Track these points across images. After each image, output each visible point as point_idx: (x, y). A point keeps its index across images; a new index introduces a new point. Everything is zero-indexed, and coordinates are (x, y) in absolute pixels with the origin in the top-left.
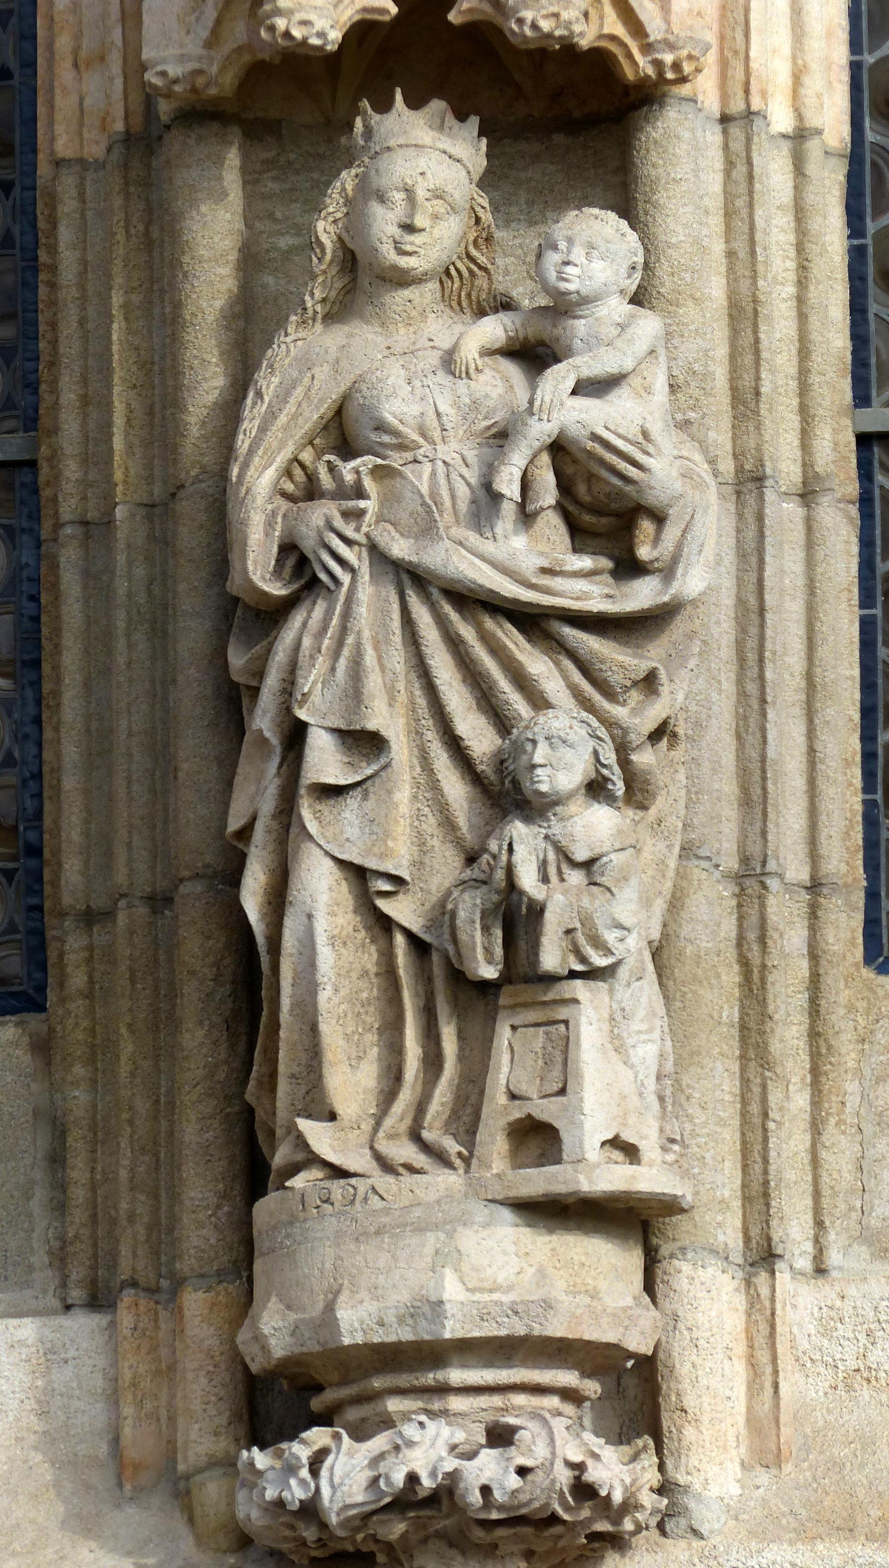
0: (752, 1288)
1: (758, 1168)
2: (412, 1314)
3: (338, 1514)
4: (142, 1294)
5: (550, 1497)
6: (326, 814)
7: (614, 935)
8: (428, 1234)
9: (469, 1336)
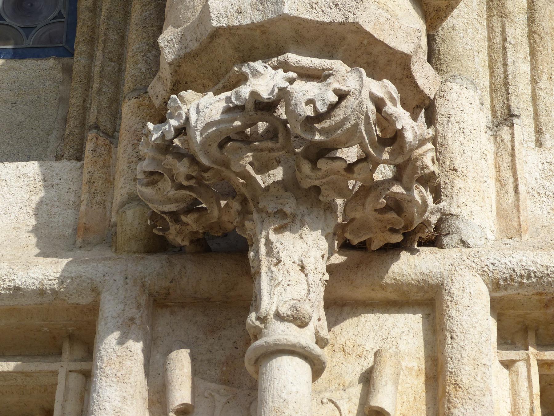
0: (499, 137)
3: (201, 135)
4: (102, 135)
5: (358, 118)
9: (302, 16)
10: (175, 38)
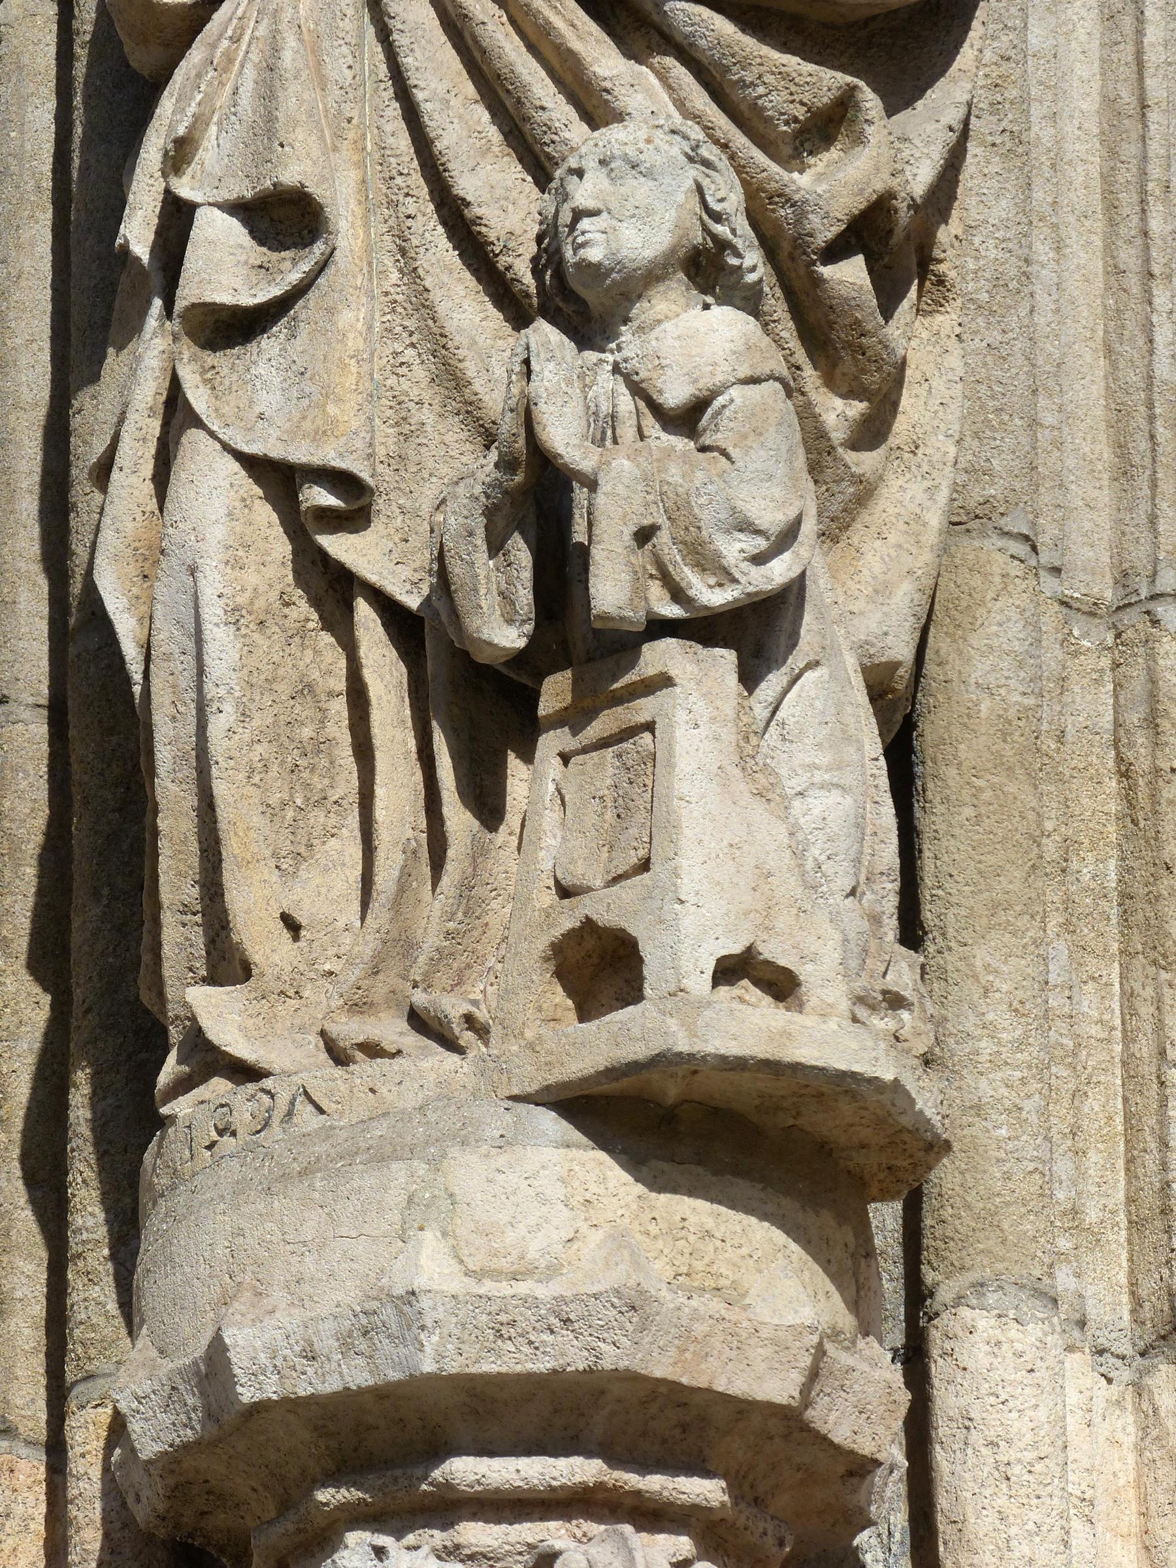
0: (1145, 1396)
1: (1151, 1162)
2: (363, 1330)
6: (225, 371)
7: (739, 546)
8: (395, 1166)
9: (473, 1370)
10: (154, 1392)
